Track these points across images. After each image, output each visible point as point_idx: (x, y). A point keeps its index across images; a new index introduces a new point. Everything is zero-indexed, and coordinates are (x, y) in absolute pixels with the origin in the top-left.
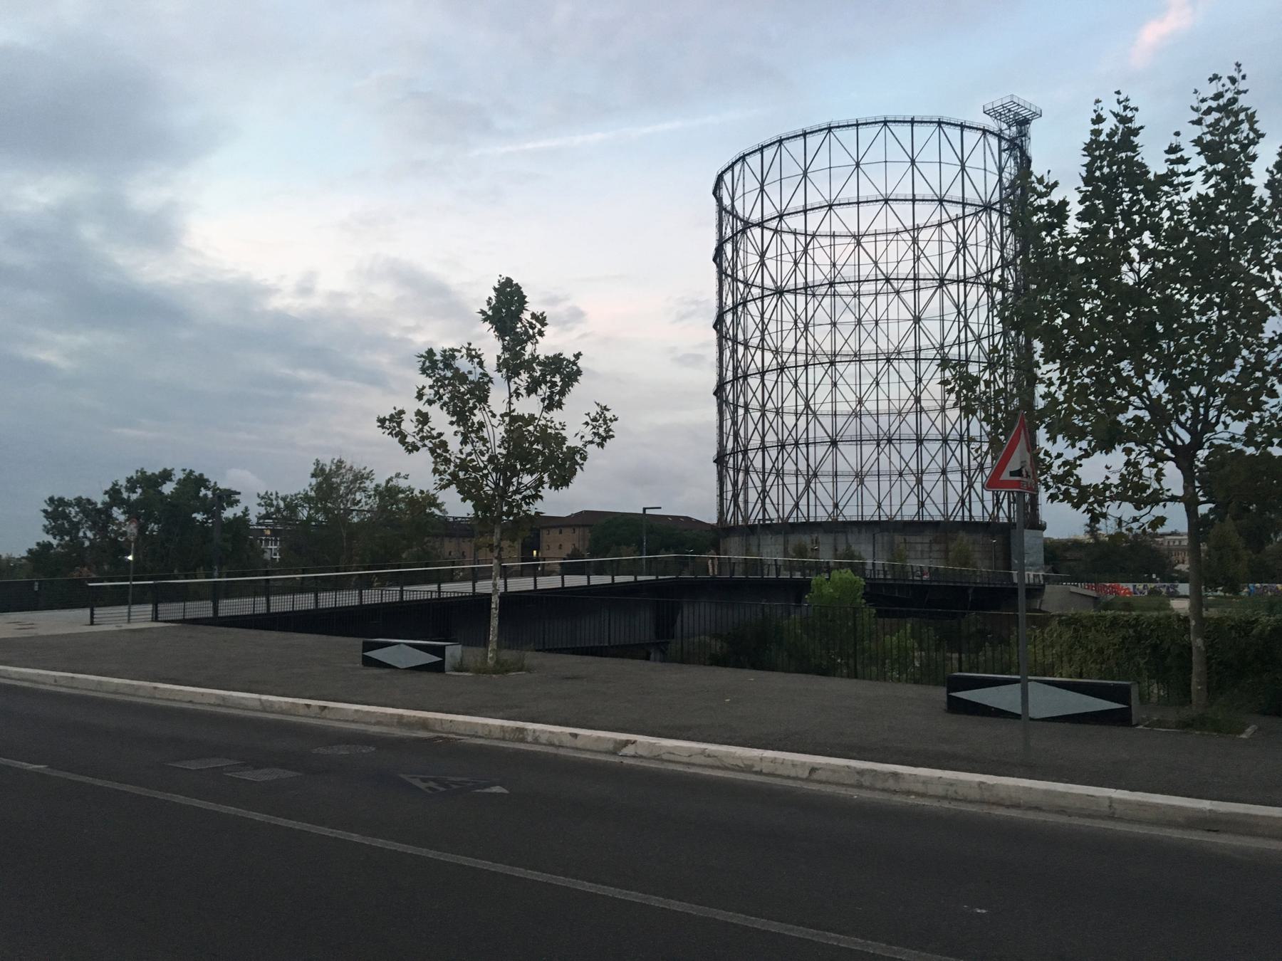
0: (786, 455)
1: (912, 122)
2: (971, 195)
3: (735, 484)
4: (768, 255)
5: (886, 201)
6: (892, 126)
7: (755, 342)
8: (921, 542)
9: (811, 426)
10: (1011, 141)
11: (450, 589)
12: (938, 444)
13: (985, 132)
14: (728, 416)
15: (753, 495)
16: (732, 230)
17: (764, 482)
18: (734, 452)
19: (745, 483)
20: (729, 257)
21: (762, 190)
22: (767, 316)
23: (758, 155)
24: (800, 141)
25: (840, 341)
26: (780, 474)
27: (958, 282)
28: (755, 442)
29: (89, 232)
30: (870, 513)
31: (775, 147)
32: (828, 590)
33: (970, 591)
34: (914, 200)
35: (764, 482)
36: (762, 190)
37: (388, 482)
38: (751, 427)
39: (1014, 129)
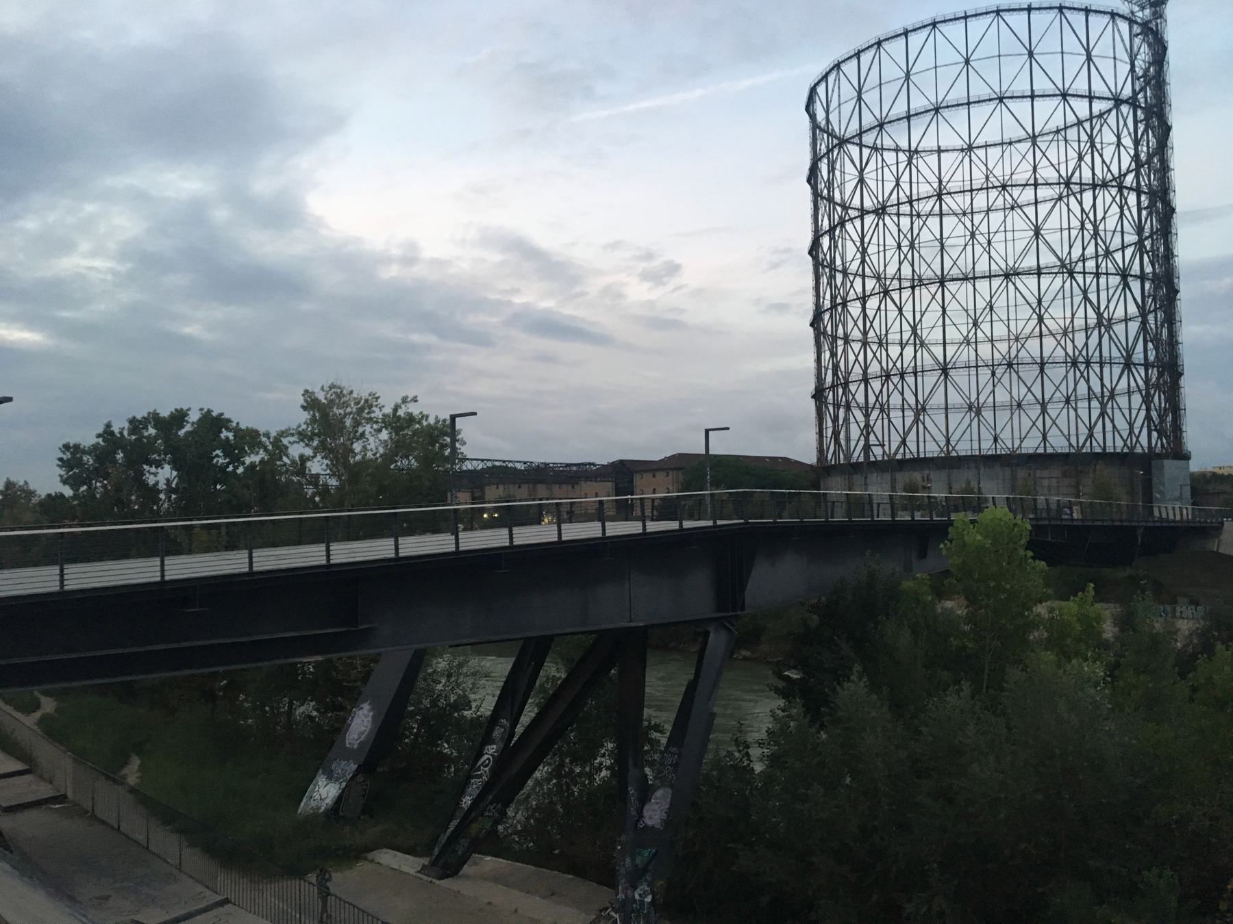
0: (891, 387)
1: (1029, 9)
2: (1099, 88)
3: (835, 420)
5: (1001, 99)
6: (1006, 16)
7: (854, 267)
8: (1049, 477)
10: (1145, 25)
11: (474, 540)
13: (1113, 15)
15: (855, 432)
16: (827, 144)
17: (867, 416)
18: (833, 387)
19: (846, 420)
20: (826, 178)
21: (860, 99)
22: (866, 240)
23: (855, 61)
24: (902, 40)
25: (948, 263)
26: (884, 409)
28: (857, 371)
29: (221, 214)
30: (987, 447)
31: (873, 51)
32: (975, 537)
33: (1140, 532)
34: (1033, 97)
35: (867, 416)
36: (860, 99)
37: (396, 409)
38: (852, 358)
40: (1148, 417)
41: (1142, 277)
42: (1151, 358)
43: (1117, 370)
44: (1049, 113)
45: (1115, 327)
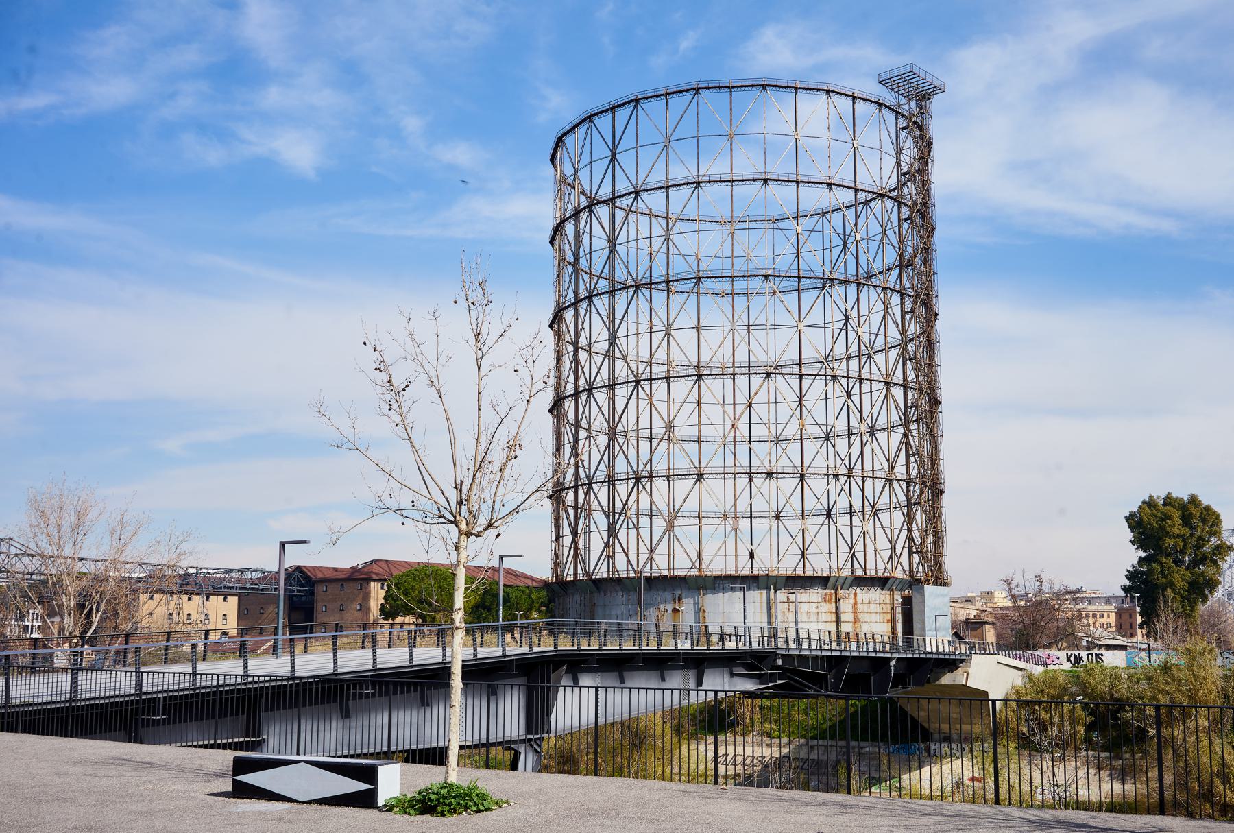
9: (867, 450)
21: (613, 157)
27: (845, 282)
31: (630, 108)
33: (893, 663)
36: (613, 157)
39: (913, 104)
40: (910, 539)
41: (905, 386)
42: (914, 474)
43: (879, 484)
44: (815, 198)
45: (878, 435)
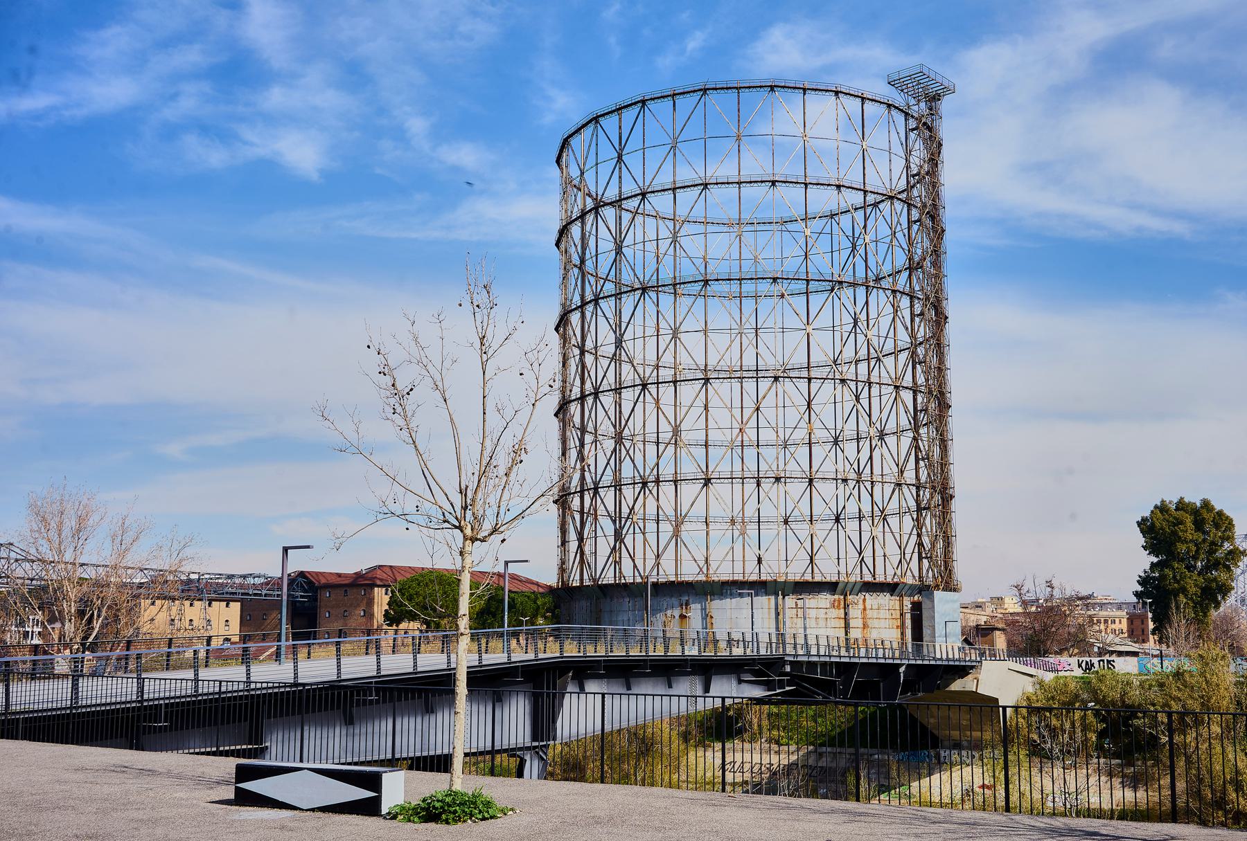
4: (625, 337)
12: (829, 446)
14: (572, 536)
21: (620, 157)
31: (637, 108)
33: (902, 669)
36: (620, 157)
39: (923, 105)
43: (888, 489)
44: (824, 200)
